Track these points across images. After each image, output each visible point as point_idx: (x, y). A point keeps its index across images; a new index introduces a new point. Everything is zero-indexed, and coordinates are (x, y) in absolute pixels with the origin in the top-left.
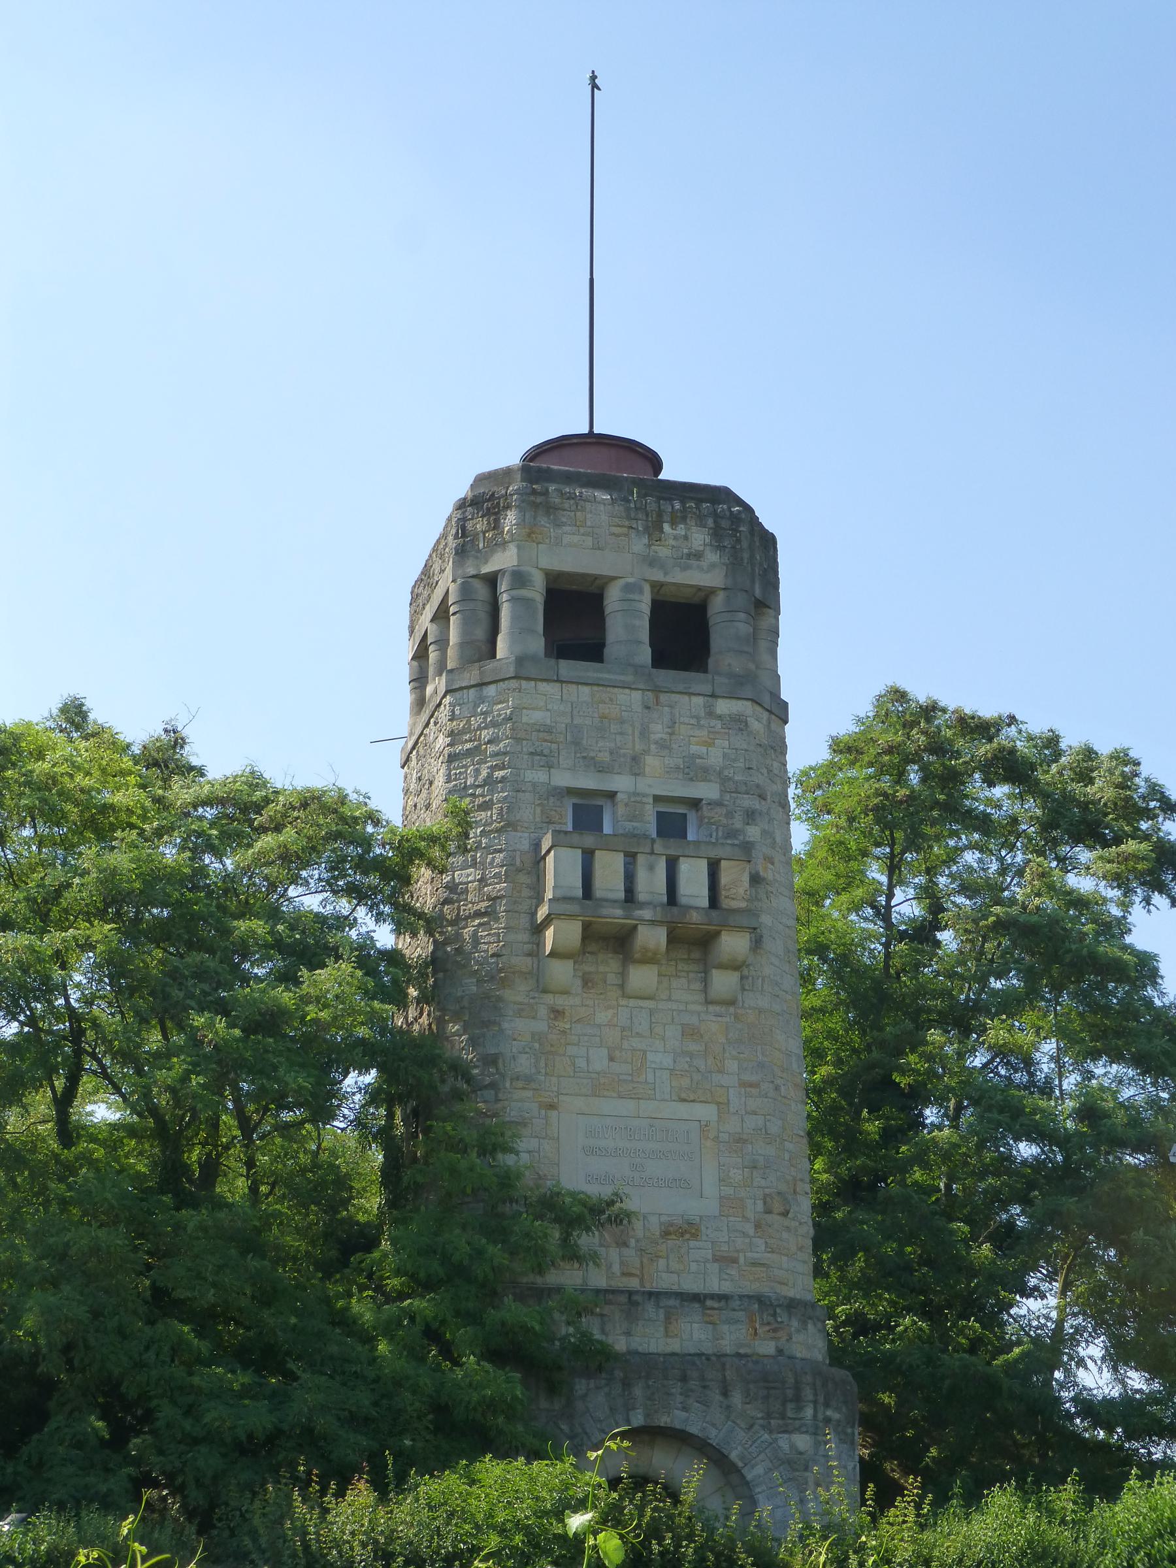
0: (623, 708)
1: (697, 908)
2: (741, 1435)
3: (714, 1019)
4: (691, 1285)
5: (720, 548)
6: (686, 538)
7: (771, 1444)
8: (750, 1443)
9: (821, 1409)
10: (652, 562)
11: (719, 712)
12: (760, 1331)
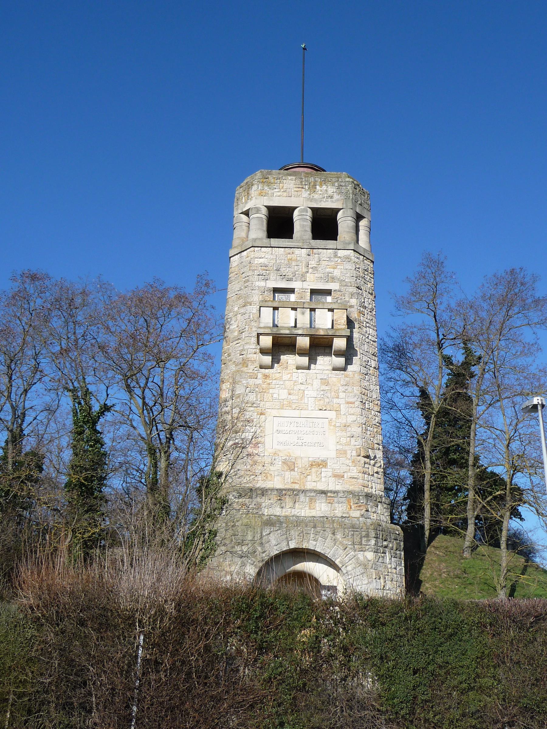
0: (298, 256)
1: (322, 329)
2: (341, 551)
3: (335, 376)
4: (321, 486)
5: (341, 193)
6: (326, 190)
7: (355, 556)
8: (345, 556)
9: (380, 541)
10: (311, 200)
11: (339, 255)
12: (353, 507)
